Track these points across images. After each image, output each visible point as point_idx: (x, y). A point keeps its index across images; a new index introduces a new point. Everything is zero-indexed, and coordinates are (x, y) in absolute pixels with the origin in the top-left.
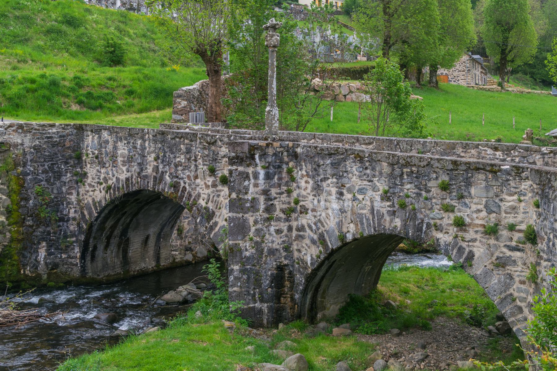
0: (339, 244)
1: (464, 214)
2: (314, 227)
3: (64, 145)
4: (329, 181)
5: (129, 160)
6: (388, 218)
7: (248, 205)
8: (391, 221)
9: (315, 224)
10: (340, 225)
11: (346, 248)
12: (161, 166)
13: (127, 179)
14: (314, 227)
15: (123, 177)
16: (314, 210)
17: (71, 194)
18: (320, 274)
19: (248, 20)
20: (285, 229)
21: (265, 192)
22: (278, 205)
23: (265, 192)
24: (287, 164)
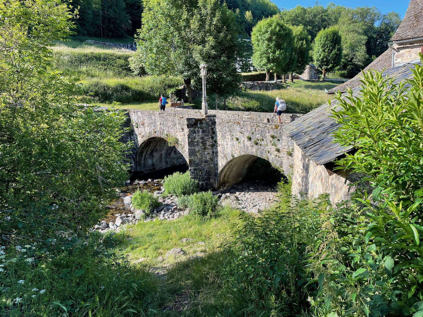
0: (232, 158)
1: (279, 146)
2: (222, 152)
3: (359, 184)
4: (228, 134)
5: (150, 124)
6: (250, 148)
7: (196, 144)
8: (251, 150)
9: (223, 151)
10: (232, 151)
11: (235, 159)
12: (162, 127)
13: (150, 132)
14: (222, 152)
15: (148, 132)
16: (222, 145)
17: (128, 138)
18: (226, 169)
19: (379, 293)
20: (211, 153)
21: (202, 138)
22: (208, 143)
23: (202, 138)
24: (211, 126)
